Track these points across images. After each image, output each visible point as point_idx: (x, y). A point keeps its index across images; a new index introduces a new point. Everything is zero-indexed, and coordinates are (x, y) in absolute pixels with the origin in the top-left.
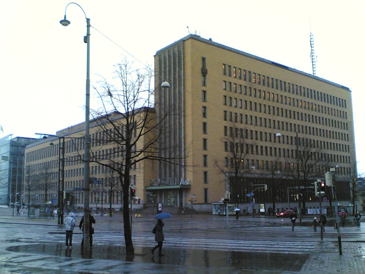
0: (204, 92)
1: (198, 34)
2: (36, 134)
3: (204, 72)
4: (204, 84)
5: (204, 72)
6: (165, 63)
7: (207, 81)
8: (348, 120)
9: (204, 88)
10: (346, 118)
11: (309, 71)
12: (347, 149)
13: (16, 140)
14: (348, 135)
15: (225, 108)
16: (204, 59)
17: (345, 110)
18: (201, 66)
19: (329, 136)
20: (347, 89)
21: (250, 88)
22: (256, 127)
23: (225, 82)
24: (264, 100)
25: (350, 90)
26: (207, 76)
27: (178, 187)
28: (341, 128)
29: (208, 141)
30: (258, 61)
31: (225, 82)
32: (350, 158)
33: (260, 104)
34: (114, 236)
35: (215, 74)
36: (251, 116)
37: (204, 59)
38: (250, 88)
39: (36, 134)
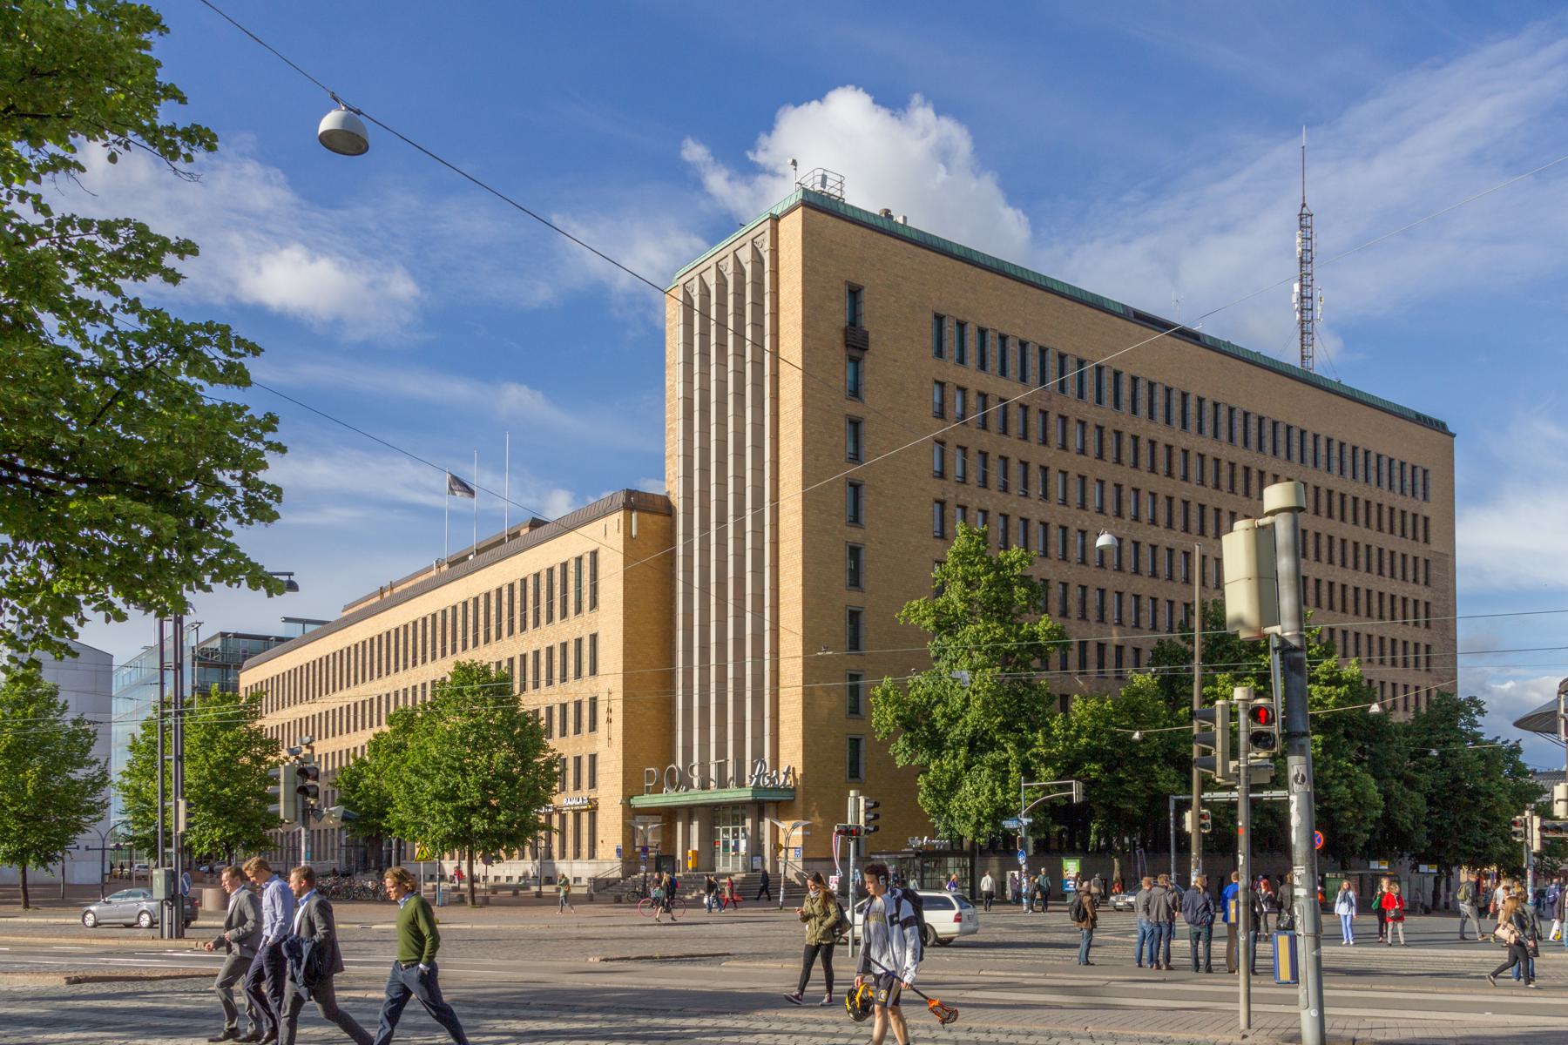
0: (855, 424)
1: (832, 189)
2: (287, 620)
3: (856, 342)
4: (855, 393)
5: (856, 342)
6: (705, 316)
7: (868, 379)
8: (1435, 545)
9: (853, 409)
10: (1426, 540)
11: (1291, 357)
12: (1420, 489)
13: (217, 644)
14: (1425, 471)
15: (936, 489)
16: (854, 293)
17: (1426, 510)
18: (842, 320)
19: (1350, 606)
20: (1440, 427)
21: (1044, 413)
22: (1063, 567)
23: (942, 385)
24: (1099, 462)
25: (1451, 430)
26: (868, 361)
27: (746, 794)
28: (1404, 578)
29: (865, 619)
30: (1077, 306)
31: (942, 385)
32: (1432, 564)
33: (1083, 478)
34: (70, 941)
35: (902, 356)
36: (1045, 525)
37: (854, 293)
38: (1044, 413)
39: (287, 620)
